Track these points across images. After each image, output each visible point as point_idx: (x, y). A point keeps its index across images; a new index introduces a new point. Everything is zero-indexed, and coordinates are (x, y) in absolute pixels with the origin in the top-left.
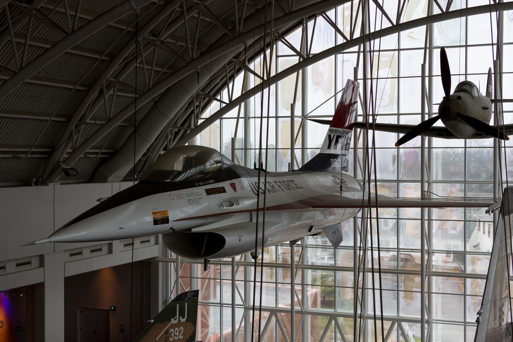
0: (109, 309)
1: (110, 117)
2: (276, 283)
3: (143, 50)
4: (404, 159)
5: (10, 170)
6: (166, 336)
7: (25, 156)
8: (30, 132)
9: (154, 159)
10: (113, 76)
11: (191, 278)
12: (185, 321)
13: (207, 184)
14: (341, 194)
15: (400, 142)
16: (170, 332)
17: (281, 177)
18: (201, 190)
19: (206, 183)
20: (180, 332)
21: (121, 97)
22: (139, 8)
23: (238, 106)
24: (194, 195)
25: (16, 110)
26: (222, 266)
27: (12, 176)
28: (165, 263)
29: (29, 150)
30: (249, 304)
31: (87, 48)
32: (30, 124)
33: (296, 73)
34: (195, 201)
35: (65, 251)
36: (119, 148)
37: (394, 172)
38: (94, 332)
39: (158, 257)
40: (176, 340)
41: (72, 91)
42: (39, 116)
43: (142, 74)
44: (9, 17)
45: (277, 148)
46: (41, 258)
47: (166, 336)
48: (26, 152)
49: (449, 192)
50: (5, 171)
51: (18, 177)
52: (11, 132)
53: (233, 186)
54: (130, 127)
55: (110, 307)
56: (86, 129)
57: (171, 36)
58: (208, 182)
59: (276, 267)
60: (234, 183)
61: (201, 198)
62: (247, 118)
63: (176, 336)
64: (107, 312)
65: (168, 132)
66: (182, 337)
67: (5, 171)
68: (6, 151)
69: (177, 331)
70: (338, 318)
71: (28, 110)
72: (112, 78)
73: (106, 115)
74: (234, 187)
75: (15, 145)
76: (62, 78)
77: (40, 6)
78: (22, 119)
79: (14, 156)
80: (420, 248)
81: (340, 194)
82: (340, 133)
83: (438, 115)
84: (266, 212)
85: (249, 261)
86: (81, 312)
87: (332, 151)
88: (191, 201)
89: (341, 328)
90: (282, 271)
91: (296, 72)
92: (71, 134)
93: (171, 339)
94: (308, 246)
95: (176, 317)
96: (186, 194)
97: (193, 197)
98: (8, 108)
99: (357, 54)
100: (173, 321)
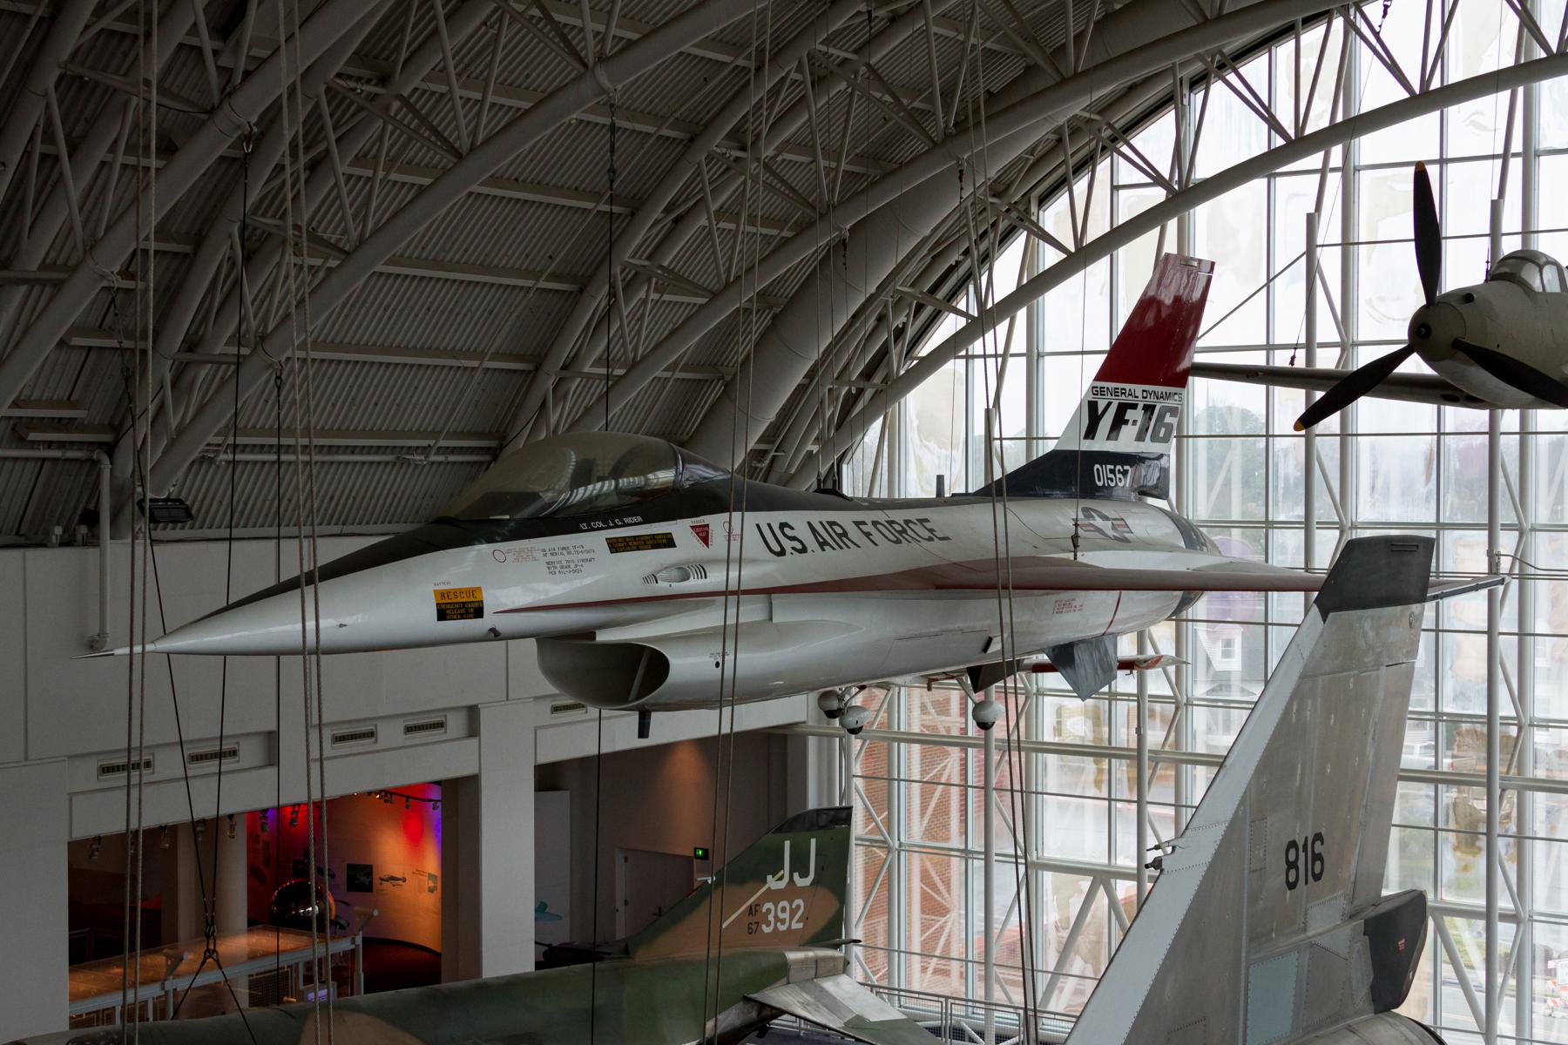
0: (690, 853)
1: (634, 358)
2: (1110, 800)
4: (1458, 465)
5: (395, 495)
6: (752, 919)
7: (422, 458)
9: (790, 465)
10: (644, 252)
12: (808, 884)
13: (616, 526)
14: (1075, 555)
15: (1308, 421)
16: (764, 910)
17: (887, 512)
18: (595, 541)
19: (614, 522)
21: (680, 307)
22: (619, 87)
24: (569, 553)
26: (1113, 761)
28: (825, 739)
29: (432, 442)
30: (1040, 854)
31: (567, 186)
33: (1158, 229)
35: (537, 698)
36: (687, 437)
39: (804, 722)
40: (782, 932)
42: (454, 358)
43: (708, 250)
44: (329, 123)
45: (1442, 431)
46: (473, 712)
47: (752, 919)
48: (425, 448)
50: (381, 494)
51: (417, 512)
53: (703, 534)
54: (712, 381)
55: (696, 849)
56: (592, 390)
58: (622, 521)
59: (1110, 756)
60: (708, 526)
62: (1034, 357)
63: (783, 921)
65: (824, 395)
66: (800, 925)
67: (381, 494)
68: (379, 447)
69: (783, 910)
70: (1113, 881)
71: (420, 343)
74: (704, 534)
76: (508, 261)
78: (412, 366)
82: (1130, 398)
85: (1189, 750)
86: (626, 860)
87: (1100, 444)
88: (558, 566)
89: (1456, 947)
91: (1159, 228)
92: (544, 404)
93: (767, 930)
94: (1195, 702)
95: (782, 872)
96: (544, 550)
97: (563, 558)
98: (365, 338)
99: (1317, 177)
100: (772, 883)
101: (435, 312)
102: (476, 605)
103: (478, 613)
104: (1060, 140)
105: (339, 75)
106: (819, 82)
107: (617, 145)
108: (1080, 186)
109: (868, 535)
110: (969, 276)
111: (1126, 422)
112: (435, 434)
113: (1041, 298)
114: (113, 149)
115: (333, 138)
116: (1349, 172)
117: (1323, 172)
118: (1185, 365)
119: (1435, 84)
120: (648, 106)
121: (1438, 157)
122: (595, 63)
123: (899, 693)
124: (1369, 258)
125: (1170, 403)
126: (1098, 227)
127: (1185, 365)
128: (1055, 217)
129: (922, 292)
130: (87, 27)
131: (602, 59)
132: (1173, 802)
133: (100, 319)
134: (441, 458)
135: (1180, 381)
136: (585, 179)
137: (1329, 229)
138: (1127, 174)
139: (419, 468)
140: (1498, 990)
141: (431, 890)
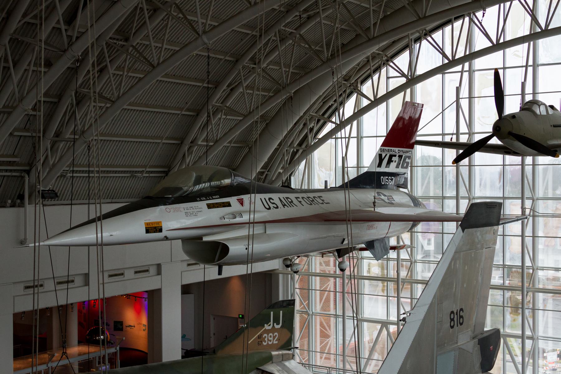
2: (387, 296)
3: (243, 79)
4: (510, 177)
6: (259, 340)
7: (141, 175)
8: (146, 154)
11: (309, 290)
13: (210, 199)
14: (374, 209)
15: (457, 161)
16: (264, 337)
18: (202, 204)
19: (209, 198)
20: (274, 338)
22: (211, 42)
23: (350, 125)
24: (193, 209)
25: (133, 135)
26: (388, 282)
27: (132, 194)
28: (285, 275)
29: (144, 169)
30: (362, 316)
32: (143, 146)
34: (193, 214)
35: (182, 261)
37: (500, 188)
38: (225, 338)
39: (278, 269)
41: (179, 116)
42: (152, 139)
44: (107, 55)
46: (159, 266)
47: (259, 340)
48: (141, 171)
49: (554, 209)
51: (139, 194)
52: (128, 154)
53: (241, 202)
54: (244, 147)
55: (239, 315)
57: (276, 63)
58: (212, 197)
59: (388, 281)
60: (243, 199)
61: (201, 211)
62: (359, 138)
63: (270, 341)
64: (236, 319)
66: (277, 342)
69: (271, 337)
72: (218, 103)
73: (213, 137)
75: (131, 165)
76: (171, 105)
77: (136, 43)
78: (137, 142)
79: (132, 175)
80: (521, 265)
81: (373, 209)
82: (394, 153)
83: (491, 134)
84: (255, 224)
85: (416, 279)
86: (214, 319)
87: (383, 169)
90: (393, 285)
97: (191, 211)
100: (267, 327)
101: (145, 123)
102: (160, 228)
103: (160, 230)
104: (368, 61)
105: (110, 38)
106: (282, 40)
107: (210, 63)
108: (376, 77)
109: (300, 202)
110: (337, 109)
111: (392, 161)
112: (145, 167)
113: (362, 117)
114: (29, 64)
115: (108, 60)
116: (471, 72)
117: (462, 72)
118: (413, 141)
119: (501, 41)
120: (221, 49)
121: (503, 67)
122: (202, 34)
123: (312, 259)
124: (478, 102)
125: (408, 154)
126: (382, 92)
127: (413, 141)
128: (367, 88)
129: (319, 115)
130: (20, 21)
131: (205, 32)
132: (410, 297)
133: (24, 126)
134: (147, 175)
135: (411, 146)
136: (199, 75)
137: (465, 92)
138: (392, 73)
139: (139, 179)
140: (526, 364)
141: (144, 330)
